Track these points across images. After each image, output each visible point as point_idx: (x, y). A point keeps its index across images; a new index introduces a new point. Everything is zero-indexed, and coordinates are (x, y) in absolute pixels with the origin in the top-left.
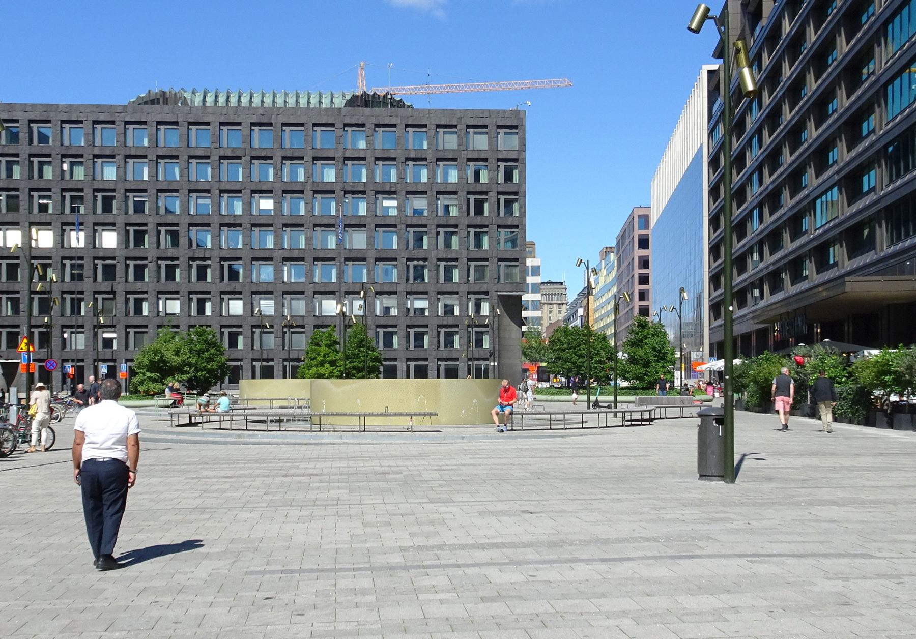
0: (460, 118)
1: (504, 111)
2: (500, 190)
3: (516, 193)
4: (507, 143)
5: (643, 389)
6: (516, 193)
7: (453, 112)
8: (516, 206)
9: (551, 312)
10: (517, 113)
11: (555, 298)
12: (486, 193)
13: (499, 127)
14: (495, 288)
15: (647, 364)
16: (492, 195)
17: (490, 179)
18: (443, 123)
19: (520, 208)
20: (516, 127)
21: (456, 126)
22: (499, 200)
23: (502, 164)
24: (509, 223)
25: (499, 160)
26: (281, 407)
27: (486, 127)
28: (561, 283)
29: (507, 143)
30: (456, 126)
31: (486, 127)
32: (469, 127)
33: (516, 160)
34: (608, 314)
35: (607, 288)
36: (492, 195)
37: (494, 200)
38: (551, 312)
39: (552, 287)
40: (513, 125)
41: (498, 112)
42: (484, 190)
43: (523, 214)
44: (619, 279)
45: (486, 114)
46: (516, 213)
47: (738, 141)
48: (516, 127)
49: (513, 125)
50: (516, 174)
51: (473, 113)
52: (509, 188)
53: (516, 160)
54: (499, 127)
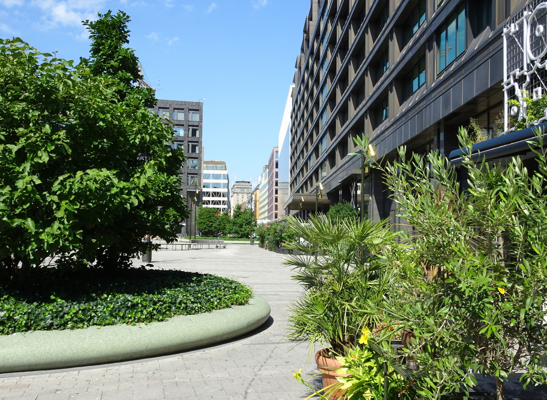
0: (171, 105)
1: (193, 103)
2: (190, 140)
3: (197, 142)
4: (194, 118)
5: (239, 238)
6: (197, 142)
7: (167, 101)
8: (197, 148)
9: (243, 197)
10: (199, 104)
11: (246, 190)
12: (182, 141)
13: (190, 110)
14: (186, 187)
15: (241, 226)
16: (186, 143)
17: (185, 135)
18: (162, 106)
19: (199, 149)
20: (198, 110)
21: (168, 108)
22: (189, 145)
23: (191, 128)
24: (193, 156)
25: (189, 126)
26: (243, 271)
27: (183, 109)
28: (249, 182)
29: (194, 118)
30: (168, 108)
31: (183, 109)
32: (175, 109)
33: (198, 126)
34: (265, 199)
35: (264, 187)
36: (186, 143)
37: (186, 144)
38: (243, 197)
39: (244, 184)
40: (197, 109)
41: (190, 102)
42: (182, 140)
43: (200, 152)
44: (269, 182)
45: (184, 104)
46: (197, 152)
47: (356, 107)
48: (198, 110)
49: (197, 109)
50: (198, 132)
51: (177, 102)
52: (194, 139)
53: (198, 126)
54: (190, 110)
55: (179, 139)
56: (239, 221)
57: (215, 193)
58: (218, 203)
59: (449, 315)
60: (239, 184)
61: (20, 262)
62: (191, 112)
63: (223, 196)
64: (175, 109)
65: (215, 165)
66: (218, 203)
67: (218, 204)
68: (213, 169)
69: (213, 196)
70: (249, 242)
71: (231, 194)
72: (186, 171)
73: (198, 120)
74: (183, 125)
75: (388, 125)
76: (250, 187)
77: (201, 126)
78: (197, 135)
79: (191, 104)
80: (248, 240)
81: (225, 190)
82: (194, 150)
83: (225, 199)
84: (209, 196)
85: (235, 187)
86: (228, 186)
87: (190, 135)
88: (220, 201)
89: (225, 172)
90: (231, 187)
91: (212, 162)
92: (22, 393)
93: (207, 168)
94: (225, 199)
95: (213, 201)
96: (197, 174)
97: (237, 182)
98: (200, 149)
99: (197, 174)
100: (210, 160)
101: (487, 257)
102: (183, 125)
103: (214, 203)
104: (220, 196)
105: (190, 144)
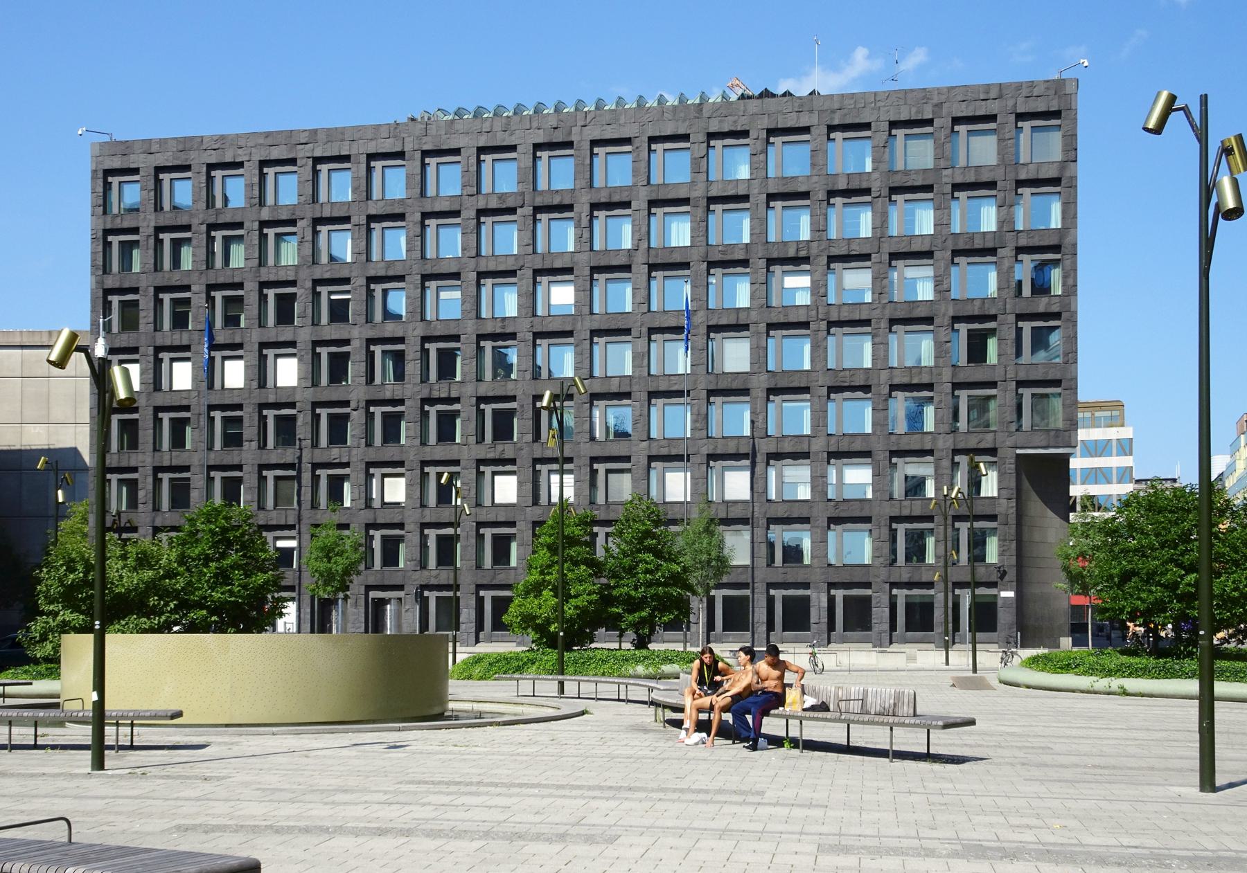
0: (939, 105)
1: (1032, 85)
10: (1058, 87)
13: (1021, 117)
16: (1006, 325)
18: (904, 116)
20: (1057, 114)
21: (930, 122)
24: (1041, 309)
27: (992, 118)
30: (930, 122)
31: (992, 118)
32: (957, 121)
36: (1006, 325)
43: (1071, 289)
45: (993, 94)
48: (1057, 114)
54: (1021, 117)
61: (572, 500)
62: (1026, 125)
64: (957, 121)
72: (1010, 375)
73: (1056, 222)
75: (90, 802)
79: (1025, 92)
92: (502, 818)
93: (1095, 424)
96: (1056, 383)
98: (1072, 340)
99: (1056, 383)
101: (669, 517)
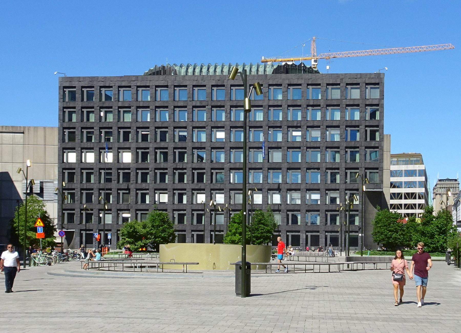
0: (342, 79)
2: (367, 124)
3: (377, 126)
4: (373, 94)
6: (377, 126)
7: (337, 75)
8: (377, 134)
10: (379, 76)
13: (367, 84)
16: (362, 128)
18: (331, 82)
19: (380, 136)
20: (378, 84)
21: (339, 84)
22: (366, 131)
27: (358, 84)
28: (456, 180)
29: (373, 94)
30: (339, 84)
31: (358, 84)
32: (347, 84)
36: (362, 128)
39: (449, 182)
40: (376, 82)
41: (366, 74)
42: (357, 124)
43: (382, 139)
46: (378, 139)
48: (378, 84)
49: (376, 82)
50: (378, 114)
52: (373, 123)
54: (367, 84)
55: (354, 124)
56: (429, 229)
57: (408, 194)
58: (412, 207)
59: (108, 250)
60: (442, 183)
63: (420, 198)
64: (347, 84)
65: (407, 159)
66: (412, 207)
67: (412, 208)
68: (407, 163)
69: (406, 198)
70: (444, 258)
71: (431, 195)
72: (363, 166)
74: (358, 105)
76: (457, 186)
77: (383, 104)
78: (378, 117)
80: (443, 255)
81: (423, 190)
82: (373, 137)
83: (422, 201)
84: (401, 198)
85: (438, 186)
86: (425, 184)
87: (368, 118)
88: (415, 205)
89: (422, 167)
90: (431, 186)
91: (404, 155)
94: (422, 201)
95: (405, 205)
96: (377, 169)
97: (440, 180)
98: (382, 135)
100: (401, 152)
102: (358, 105)
103: (407, 207)
104: (415, 198)
105: (368, 129)
